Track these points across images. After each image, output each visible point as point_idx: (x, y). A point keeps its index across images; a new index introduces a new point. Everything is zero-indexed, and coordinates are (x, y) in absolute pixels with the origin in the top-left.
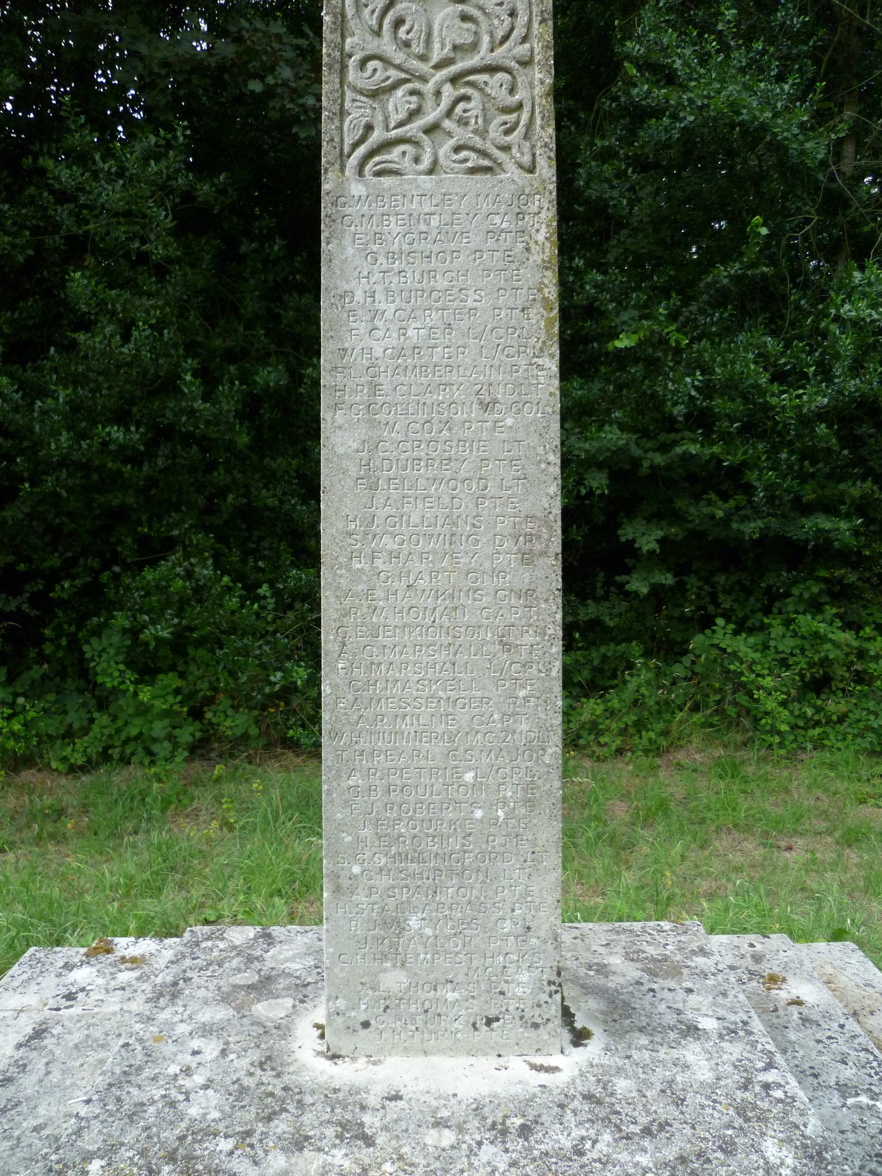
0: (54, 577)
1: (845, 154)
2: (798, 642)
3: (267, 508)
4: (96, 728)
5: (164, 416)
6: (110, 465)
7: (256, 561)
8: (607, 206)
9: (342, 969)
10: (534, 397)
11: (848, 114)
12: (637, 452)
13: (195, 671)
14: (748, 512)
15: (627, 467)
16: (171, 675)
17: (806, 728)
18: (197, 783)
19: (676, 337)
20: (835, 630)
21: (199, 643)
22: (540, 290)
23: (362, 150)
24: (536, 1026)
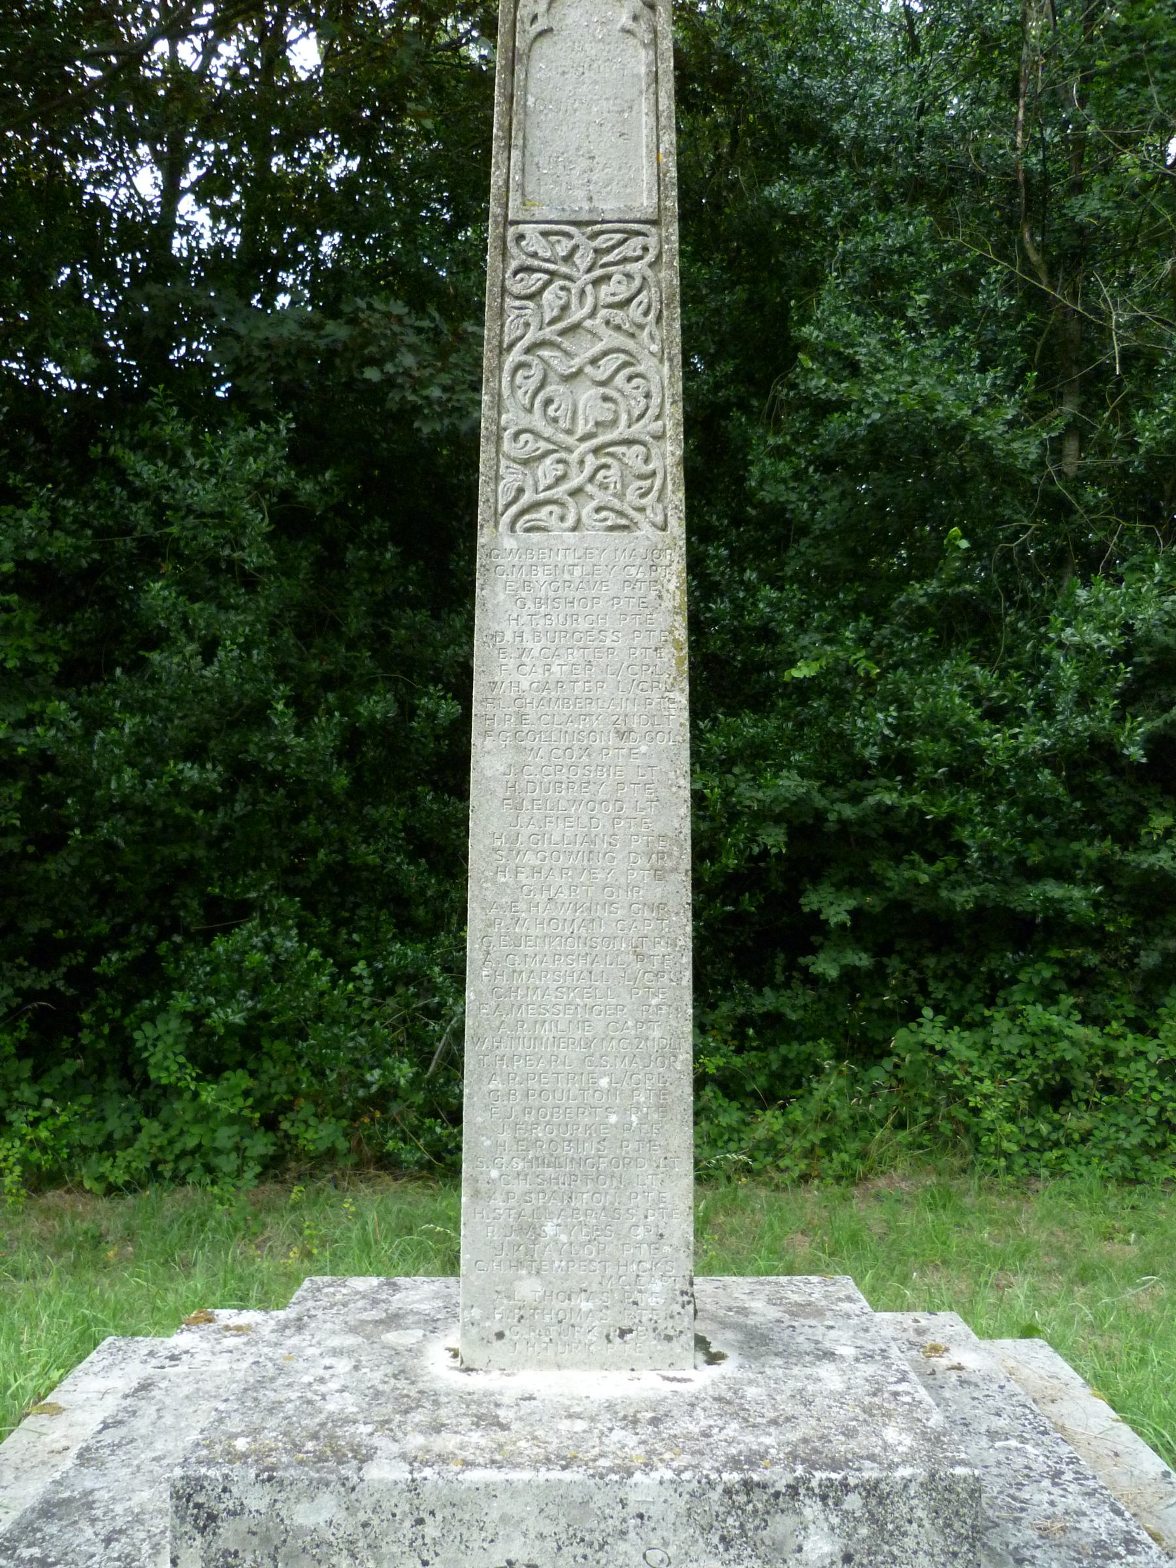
0: (97, 949)
1: (1066, 452)
2: (1027, 1039)
3: (366, 866)
4: (143, 1138)
5: (247, 751)
6: (178, 810)
7: (350, 934)
8: (785, 510)
9: (478, 1276)
10: (666, 728)
11: (1067, 408)
12: (820, 802)
13: (270, 1068)
14: (961, 877)
15: (810, 821)
16: (240, 1072)
17: (1040, 1151)
18: (270, 1208)
19: (866, 667)
20: (1073, 1025)
21: (275, 1035)
22: (671, 632)
23: (514, 509)
24: (669, 1338)
